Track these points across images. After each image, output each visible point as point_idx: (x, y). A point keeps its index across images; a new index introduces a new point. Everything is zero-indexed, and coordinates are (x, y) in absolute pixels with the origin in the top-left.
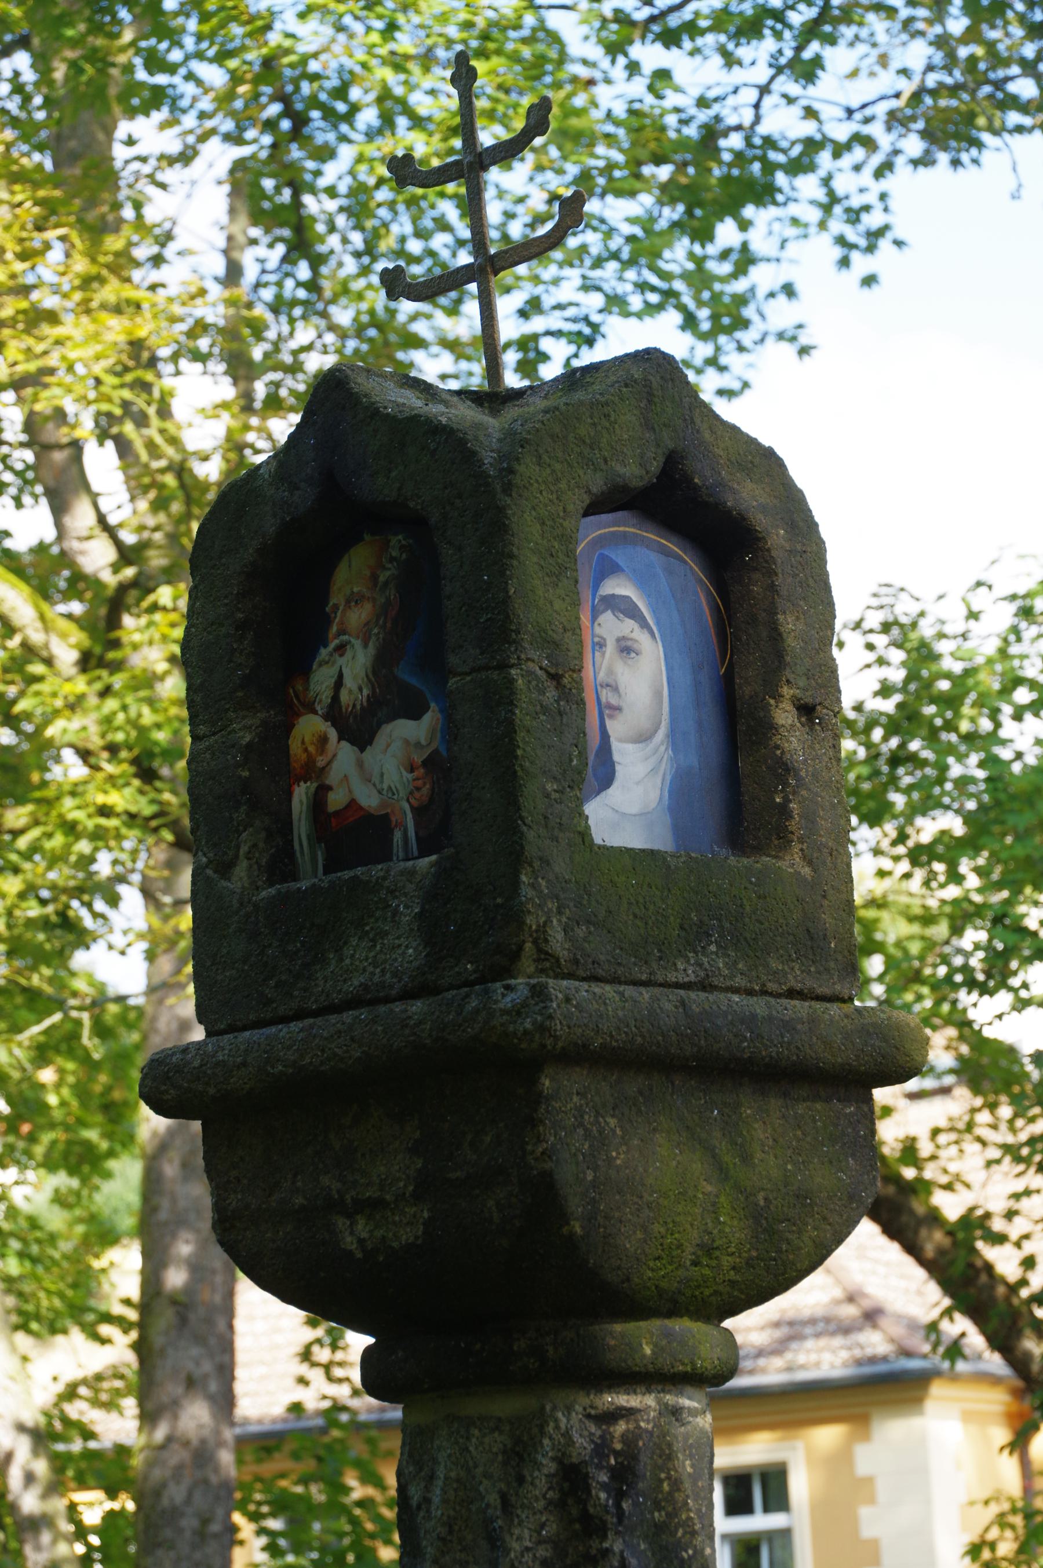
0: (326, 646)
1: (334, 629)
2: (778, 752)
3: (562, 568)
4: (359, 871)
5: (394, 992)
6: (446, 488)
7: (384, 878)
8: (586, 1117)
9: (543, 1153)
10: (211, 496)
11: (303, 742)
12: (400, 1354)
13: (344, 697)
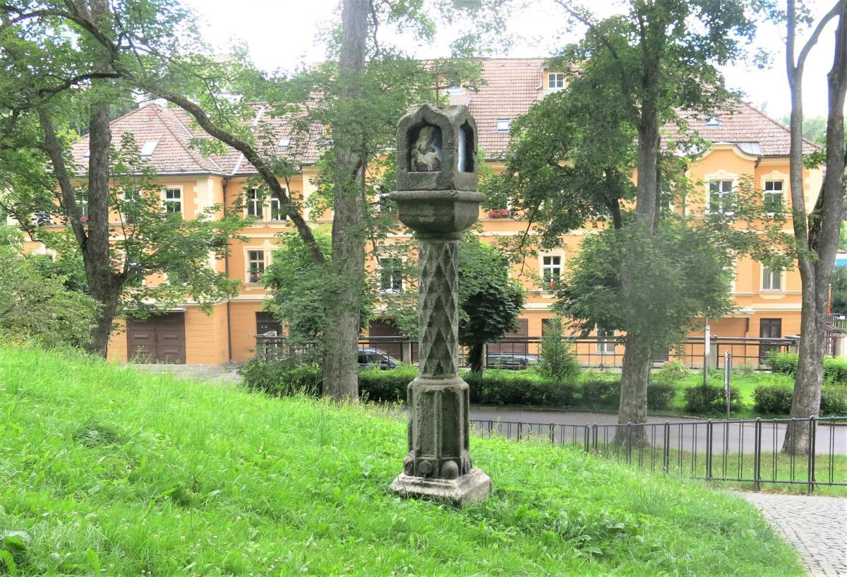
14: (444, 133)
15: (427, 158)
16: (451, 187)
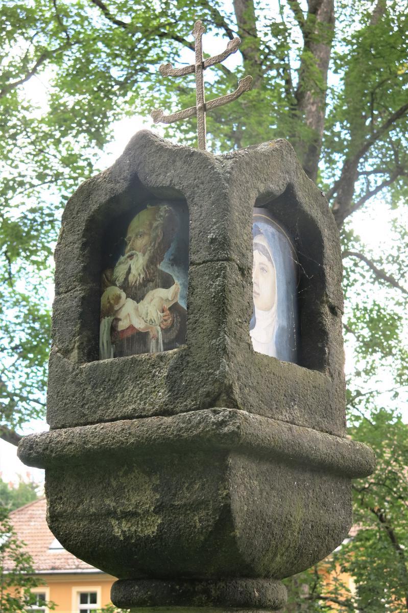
0: (123, 255)
1: (128, 247)
2: (321, 325)
3: (245, 223)
4: (136, 356)
5: (151, 413)
6: (195, 180)
7: (149, 359)
8: (246, 479)
9: (226, 495)
10: (59, 214)
11: (108, 299)
12: (137, 587)
13: (131, 278)
14: (194, 210)
15: (144, 313)
16: (221, 395)
